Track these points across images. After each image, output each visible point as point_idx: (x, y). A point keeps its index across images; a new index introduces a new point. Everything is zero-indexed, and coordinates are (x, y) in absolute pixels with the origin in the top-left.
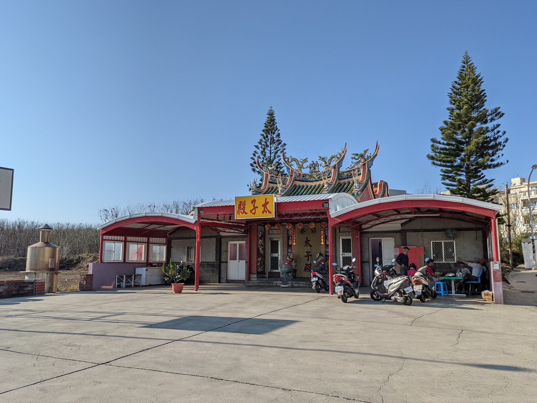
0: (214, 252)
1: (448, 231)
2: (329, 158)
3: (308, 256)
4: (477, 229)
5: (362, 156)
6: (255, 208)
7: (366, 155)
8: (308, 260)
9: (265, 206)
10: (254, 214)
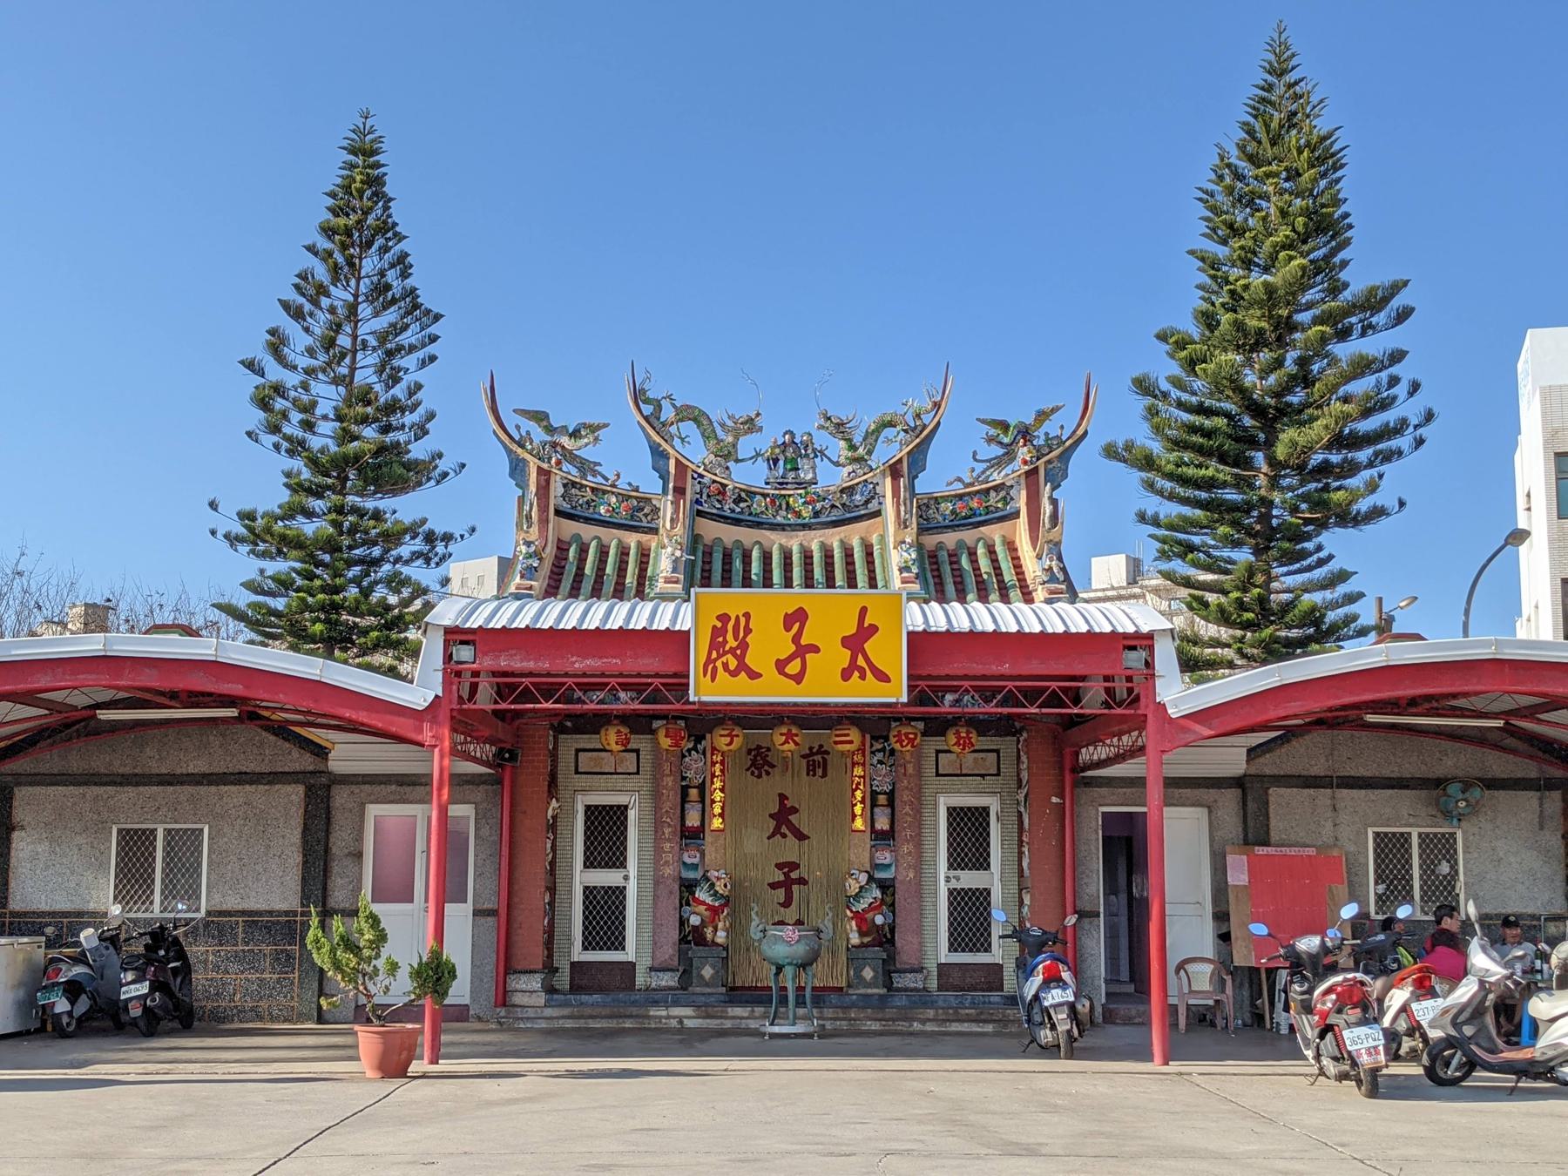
0: (296, 858)
1: (1453, 789)
2: (869, 422)
3: (787, 884)
4: (1547, 785)
5: (1025, 433)
7: (1041, 433)
8: (787, 903)
9: (856, 642)
10: (798, 678)
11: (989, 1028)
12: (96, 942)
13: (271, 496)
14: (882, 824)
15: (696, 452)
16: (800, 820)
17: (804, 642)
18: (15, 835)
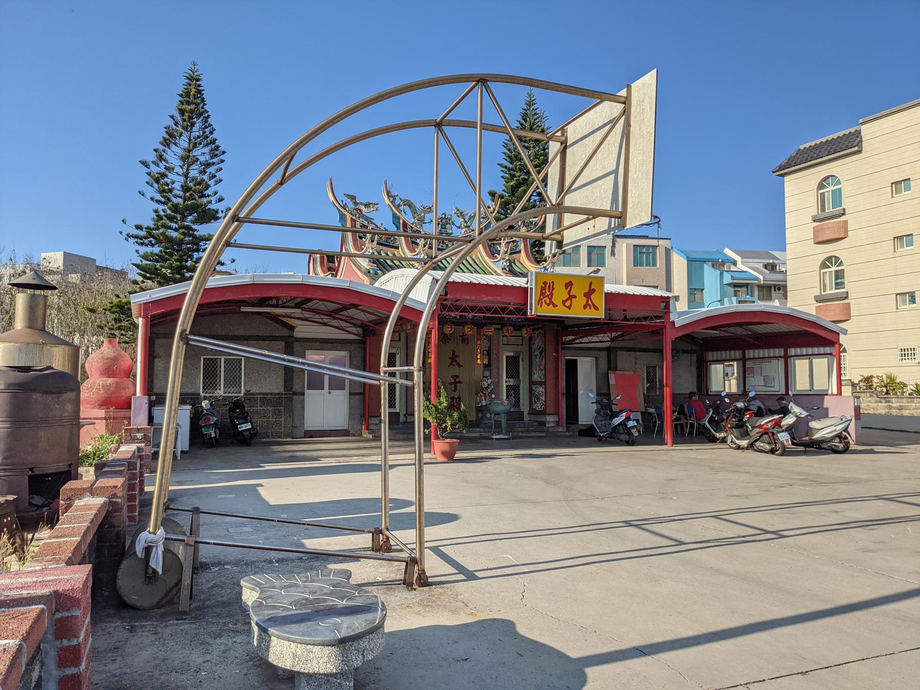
3: (455, 383)
6: (571, 297)
9: (588, 295)
10: (569, 308)
11: (544, 434)
12: (209, 407)
13: (148, 221)
14: (486, 362)
15: (409, 218)
16: (460, 360)
17: (572, 294)
18: (156, 360)
